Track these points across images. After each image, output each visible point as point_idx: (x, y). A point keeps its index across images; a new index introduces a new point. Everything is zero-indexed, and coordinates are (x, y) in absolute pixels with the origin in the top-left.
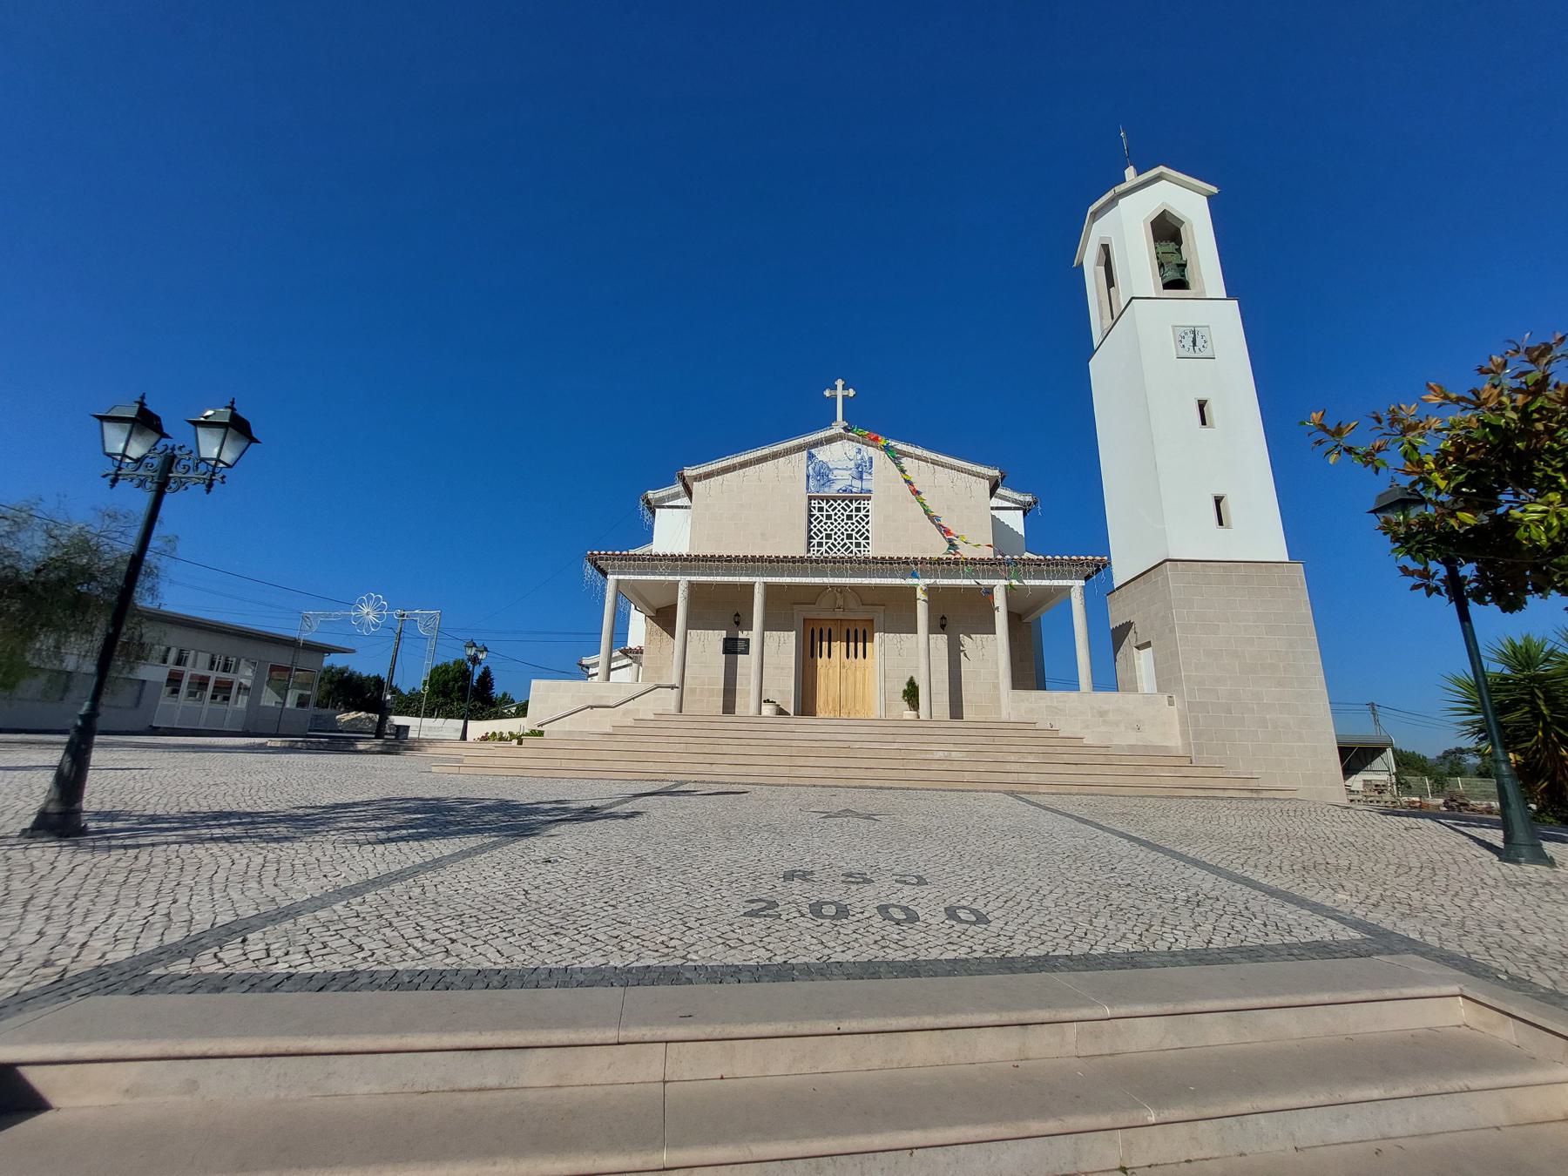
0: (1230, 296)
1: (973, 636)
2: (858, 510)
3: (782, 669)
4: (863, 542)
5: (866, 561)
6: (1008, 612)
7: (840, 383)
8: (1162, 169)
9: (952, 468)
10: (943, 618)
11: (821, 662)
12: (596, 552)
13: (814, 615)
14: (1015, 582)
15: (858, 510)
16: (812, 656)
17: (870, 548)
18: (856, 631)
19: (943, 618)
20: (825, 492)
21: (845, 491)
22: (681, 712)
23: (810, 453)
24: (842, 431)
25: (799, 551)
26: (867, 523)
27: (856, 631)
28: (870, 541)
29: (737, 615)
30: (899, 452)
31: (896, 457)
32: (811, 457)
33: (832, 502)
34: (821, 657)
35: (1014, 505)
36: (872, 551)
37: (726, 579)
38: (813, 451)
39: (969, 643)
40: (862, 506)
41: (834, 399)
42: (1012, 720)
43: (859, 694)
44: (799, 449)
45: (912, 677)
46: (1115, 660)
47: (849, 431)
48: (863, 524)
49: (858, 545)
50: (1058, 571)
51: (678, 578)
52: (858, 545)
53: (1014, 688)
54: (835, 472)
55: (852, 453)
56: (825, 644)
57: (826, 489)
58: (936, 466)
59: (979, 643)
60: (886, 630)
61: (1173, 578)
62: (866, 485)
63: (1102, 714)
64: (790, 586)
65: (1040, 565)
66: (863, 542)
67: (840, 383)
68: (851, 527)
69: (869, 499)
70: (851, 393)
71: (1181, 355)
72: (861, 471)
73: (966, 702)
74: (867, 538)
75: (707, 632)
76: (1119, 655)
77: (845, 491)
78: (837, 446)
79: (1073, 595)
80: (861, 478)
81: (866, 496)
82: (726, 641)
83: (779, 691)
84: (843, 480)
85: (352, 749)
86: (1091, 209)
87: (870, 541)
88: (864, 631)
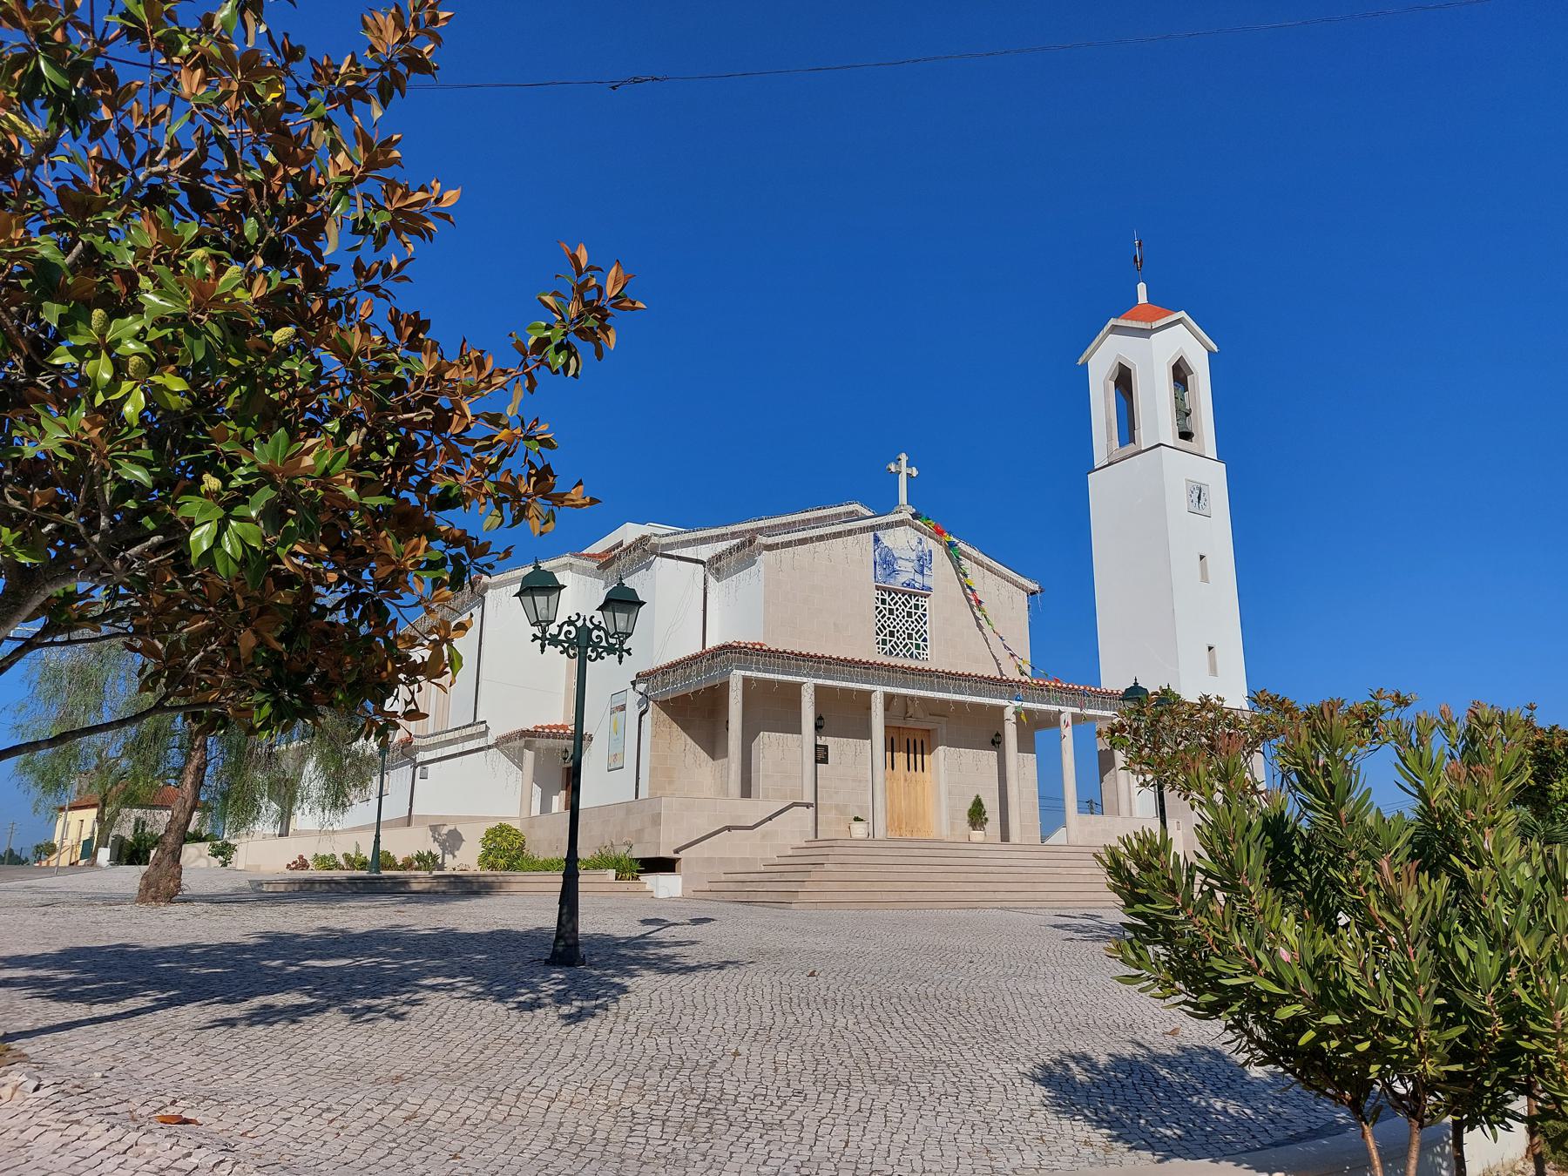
0: (150, 449)
3: (860, 781)
4: (922, 644)
7: (904, 457)
15: (916, 607)
17: (928, 651)
18: (915, 741)
20: (890, 584)
21: (908, 585)
22: (816, 837)
23: (875, 535)
24: (910, 518)
26: (925, 623)
27: (915, 741)
28: (928, 644)
32: (877, 540)
33: (893, 595)
40: (920, 603)
42: (1079, 844)
44: (863, 530)
46: (1102, 781)
47: (917, 519)
48: (922, 623)
49: (918, 646)
50: (970, 687)
52: (918, 646)
53: (1079, 812)
54: (900, 562)
55: (914, 543)
57: (892, 581)
62: (927, 582)
66: (922, 644)
67: (904, 457)
68: (911, 624)
69: (926, 596)
70: (893, 467)
72: (923, 563)
74: (925, 640)
75: (786, 735)
76: (1106, 777)
77: (908, 585)
79: (804, 693)
80: (922, 573)
81: (926, 592)
83: (858, 806)
84: (906, 572)
86: (1112, 322)
87: (928, 644)
88: (922, 742)
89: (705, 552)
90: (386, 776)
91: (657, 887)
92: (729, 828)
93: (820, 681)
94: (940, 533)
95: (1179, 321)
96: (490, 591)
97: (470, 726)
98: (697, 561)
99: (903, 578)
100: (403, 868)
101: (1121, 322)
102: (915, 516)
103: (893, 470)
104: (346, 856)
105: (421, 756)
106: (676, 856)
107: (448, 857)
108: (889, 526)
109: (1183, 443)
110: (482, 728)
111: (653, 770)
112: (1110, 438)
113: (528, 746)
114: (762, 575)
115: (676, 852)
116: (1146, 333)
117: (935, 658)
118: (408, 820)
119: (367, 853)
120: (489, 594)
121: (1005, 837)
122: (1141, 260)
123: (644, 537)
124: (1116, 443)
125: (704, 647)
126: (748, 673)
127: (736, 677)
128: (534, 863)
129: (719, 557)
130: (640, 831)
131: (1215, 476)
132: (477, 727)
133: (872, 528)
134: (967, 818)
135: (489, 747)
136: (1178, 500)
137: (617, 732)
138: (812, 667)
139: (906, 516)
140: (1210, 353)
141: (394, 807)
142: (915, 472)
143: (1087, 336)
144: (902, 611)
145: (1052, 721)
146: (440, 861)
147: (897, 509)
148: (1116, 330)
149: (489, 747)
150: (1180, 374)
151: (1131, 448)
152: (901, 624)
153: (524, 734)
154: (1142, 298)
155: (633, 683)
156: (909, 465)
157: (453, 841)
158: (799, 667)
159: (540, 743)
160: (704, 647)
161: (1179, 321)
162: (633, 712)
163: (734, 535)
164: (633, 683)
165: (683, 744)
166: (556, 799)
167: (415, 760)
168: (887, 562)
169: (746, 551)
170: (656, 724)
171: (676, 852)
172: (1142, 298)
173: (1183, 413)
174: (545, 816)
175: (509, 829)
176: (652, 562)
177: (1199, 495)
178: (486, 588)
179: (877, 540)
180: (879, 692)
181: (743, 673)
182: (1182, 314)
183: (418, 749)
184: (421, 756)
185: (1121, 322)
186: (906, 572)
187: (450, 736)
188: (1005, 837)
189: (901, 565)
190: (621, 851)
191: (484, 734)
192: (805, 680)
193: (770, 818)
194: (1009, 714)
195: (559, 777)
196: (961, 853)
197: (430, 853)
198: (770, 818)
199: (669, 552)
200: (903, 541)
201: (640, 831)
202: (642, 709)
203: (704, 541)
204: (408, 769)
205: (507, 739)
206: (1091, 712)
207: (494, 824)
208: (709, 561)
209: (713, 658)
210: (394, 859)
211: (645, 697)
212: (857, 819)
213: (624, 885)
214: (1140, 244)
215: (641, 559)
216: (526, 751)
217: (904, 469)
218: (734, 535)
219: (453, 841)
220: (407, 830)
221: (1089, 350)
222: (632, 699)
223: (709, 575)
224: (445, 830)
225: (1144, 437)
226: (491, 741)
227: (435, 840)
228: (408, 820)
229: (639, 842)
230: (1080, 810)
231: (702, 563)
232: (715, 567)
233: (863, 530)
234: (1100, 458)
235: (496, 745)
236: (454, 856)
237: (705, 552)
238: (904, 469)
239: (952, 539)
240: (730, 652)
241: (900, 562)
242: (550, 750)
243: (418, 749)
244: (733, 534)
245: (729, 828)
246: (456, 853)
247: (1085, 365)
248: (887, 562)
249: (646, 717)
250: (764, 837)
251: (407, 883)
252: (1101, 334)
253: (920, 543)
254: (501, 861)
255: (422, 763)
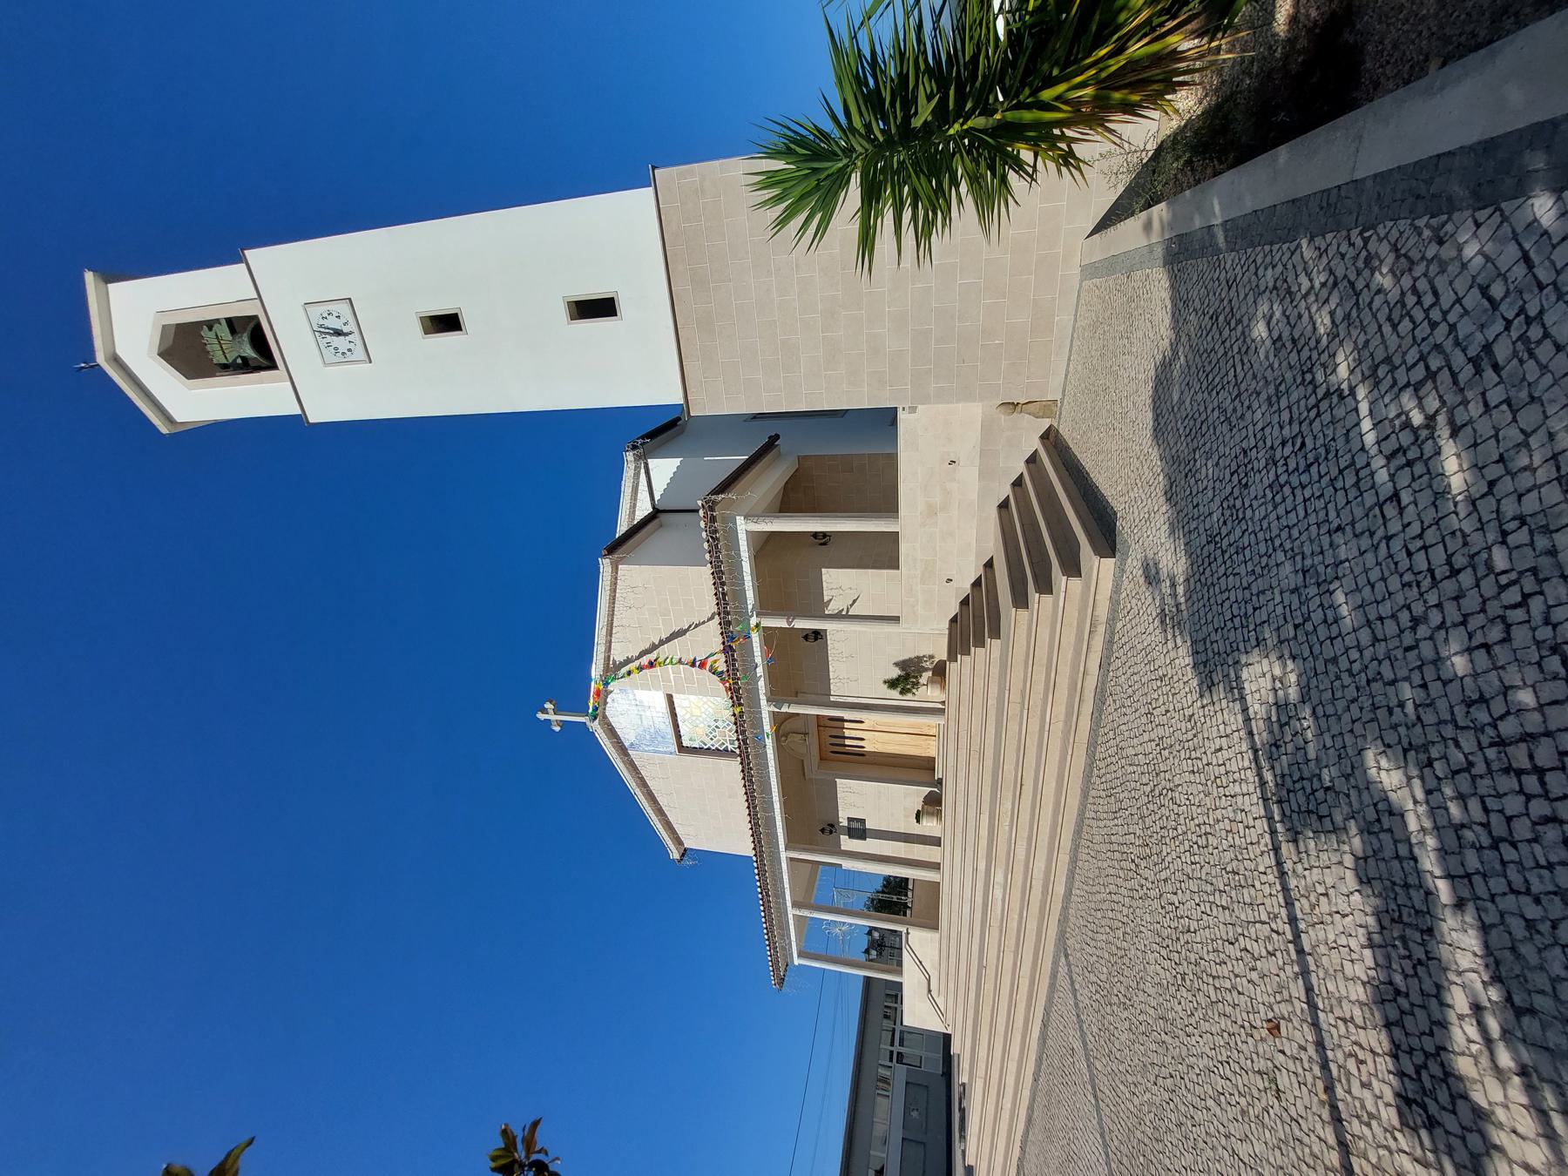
1: (826, 599)
8: (100, 358)
11: (869, 747)
12: (766, 937)
13: (815, 751)
16: (863, 755)
29: (823, 831)
30: (607, 668)
34: (863, 747)
35: (643, 471)
37: (777, 806)
41: (563, 724)
45: (885, 682)
51: (790, 916)
56: (848, 742)
58: (615, 624)
59: (833, 593)
63: (932, 512)
64: (784, 792)
65: (724, 594)
67: (541, 716)
71: (363, 356)
73: (930, 850)
82: (851, 837)
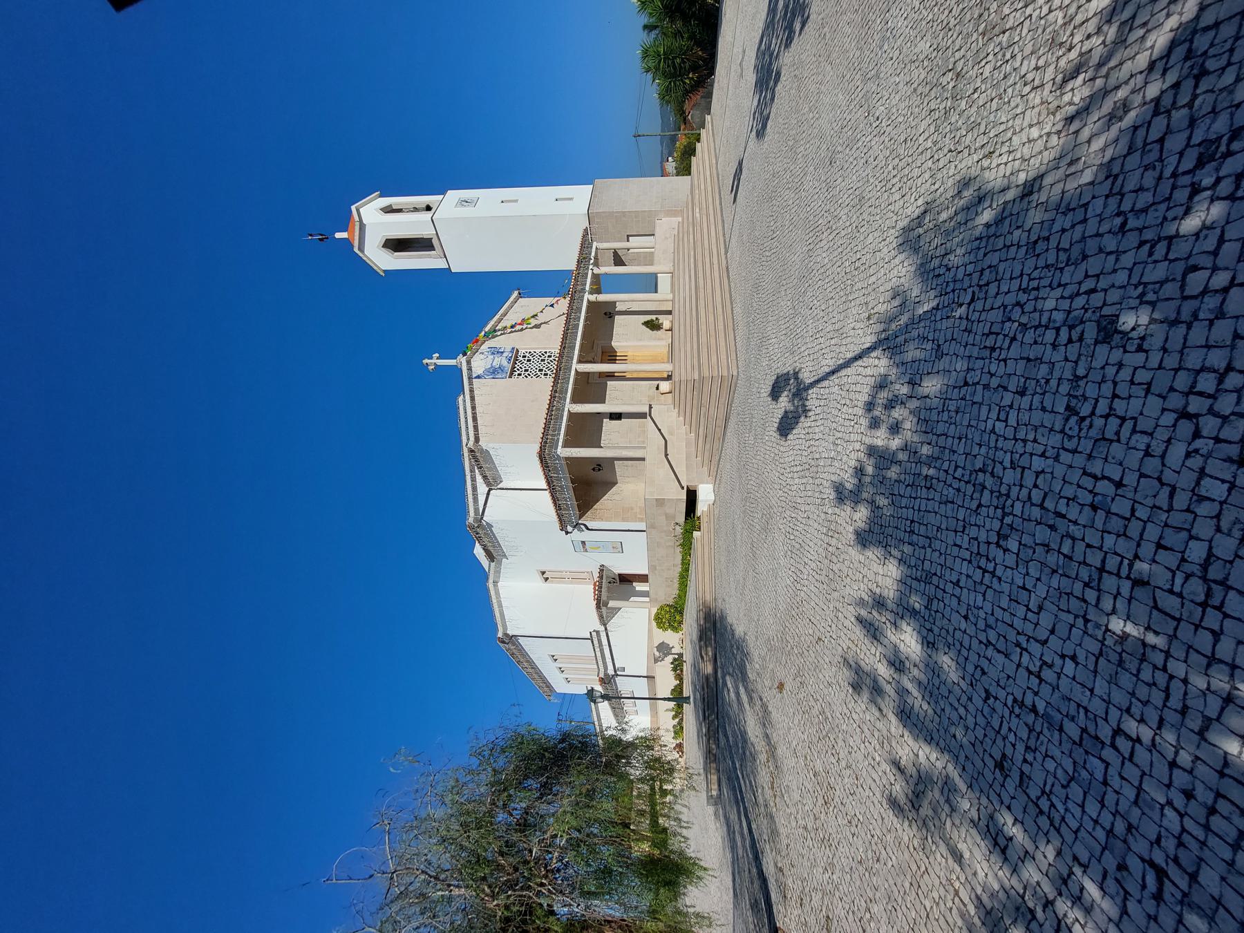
2: (524, 357)
4: (548, 354)
5: (561, 355)
6: (589, 373)
7: (426, 361)
9: (511, 307)
10: (605, 314)
14: (592, 262)
17: (553, 351)
19: (605, 314)
23: (476, 378)
25: (549, 381)
31: (492, 334)
32: (478, 377)
36: (556, 350)
38: (474, 376)
39: (619, 307)
43: (650, 358)
44: (471, 383)
52: (550, 356)
54: (494, 364)
55: (482, 356)
60: (610, 336)
61: (593, 210)
67: (426, 361)
69: (518, 351)
70: (431, 367)
72: (496, 352)
74: (546, 352)
78: (473, 364)
80: (502, 352)
85: (712, 679)
86: (356, 250)
89: (482, 488)
90: (623, 696)
91: (706, 501)
92: (666, 455)
93: (568, 400)
94: (477, 341)
95: (358, 211)
96: (508, 632)
97: (592, 642)
98: (488, 494)
99: (505, 363)
100: (681, 680)
101: (356, 244)
102: (465, 354)
103: (433, 367)
104: (674, 718)
105: (611, 672)
106: (685, 488)
107: (674, 651)
108: (470, 369)
109: (433, 211)
110: (594, 634)
111: (624, 520)
112: (430, 257)
113: (606, 604)
114: (496, 446)
115: (683, 488)
116: (362, 227)
117: (554, 347)
118: (650, 678)
119: (672, 704)
120: (510, 632)
121: (669, 313)
122: (322, 235)
123: (600, 681)
124: (433, 252)
125: (546, 490)
126: (560, 444)
127: (563, 452)
128: (679, 596)
129: (485, 477)
130: (667, 516)
131: (453, 195)
132: (594, 638)
133: (470, 378)
134: (655, 332)
135: (606, 629)
136: (467, 211)
137: (598, 546)
138: (558, 402)
139: (463, 360)
140: (381, 196)
141: (641, 688)
142: (437, 355)
143: (366, 268)
144: (526, 365)
145: (596, 277)
146: (677, 656)
147: (459, 366)
148: (361, 248)
149: (606, 629)
150: (389, 210)
151: (435, 242)
152: (535, 365)
153: (598, 607)
154: (344, 235)
155: (567, 533)
156: (432, 358)
157: (664, 649)
158: (558, 409)
159: (604, 598)
160: (546, 490)
161: (358, 211)
162: (586, 536)
163: (472, 471)
164: (567, 533)
165: (608, 501)
166: (637, 589)
167: (613, 676)
168: (494, 372)
169: (481, 459)
170: (594, 519)
171: (683, 488)
172: (344, 235)
173: (416, 210)
174: (651, 594)
175: (657, 614)
176: (487, 523)
177: (465, 202)
178: (506, 635)
179: (478, 377)
180: (576, 366)
181: (559, 447)
182: (353, 208)
183: (606, 674)
184: (611, 672)
185: (356, 244)
186: (498, 361)
187: (599, 654)
188: (669, 313)
189: (496, 364)
190: (679, 530)
191: (598, 632)
192: (566, 409)
193: (660, 430)
194: (593, 298)
195: (625, 587)
196: (682, 310)
197: (672, 663)
198: (660, 430)
199: (481, 512)
200: (480, 363)
201: (667, 516)
202: (584, 528)
203: (474, 489)
204: (618, 679)
205: (601, 617)
206: (593, 254)
207: (654, 624)
208: (488, 485)
209: (548, 467)
210: (676, 686)
211: (576, 526)
212: (657, 388)
213: (704, 525)
214: (311, 235)
215: (484, 528)
216: (609, 606)
217: (434, 361)
218: (473, 479)
219: (664, 649)
220: (658, 680)
221: (375, 268)
222: (577, 535)
223: (499, 487)
224: (657, 654)
225: (426, 232)
226: (602, 628)
227: (663, 660)
228: (650, 678)
229: (674, 517)
230: (652, 265)
231: (489, 491)
232: (493, 482)
233: (471, 383)
234: (441, 264)
235: (605, 625)
236: (673, 647)
237: (482, 488)
238: (434, 361)
239: (483, 333)
240: (545, 459)
241: (494, 364)
242: (609, 590)
243: (606, 674)
244: (471, 471)
245: (666, 455)
246: (671, 646)
247: (385, 271)
248: (494, 372)
249: (590, 525)
250: (671, 434)
251: (707, 678)
252: (365, 258)
253: (483, 353)
254: (678, 618)
255: (615, 671)
